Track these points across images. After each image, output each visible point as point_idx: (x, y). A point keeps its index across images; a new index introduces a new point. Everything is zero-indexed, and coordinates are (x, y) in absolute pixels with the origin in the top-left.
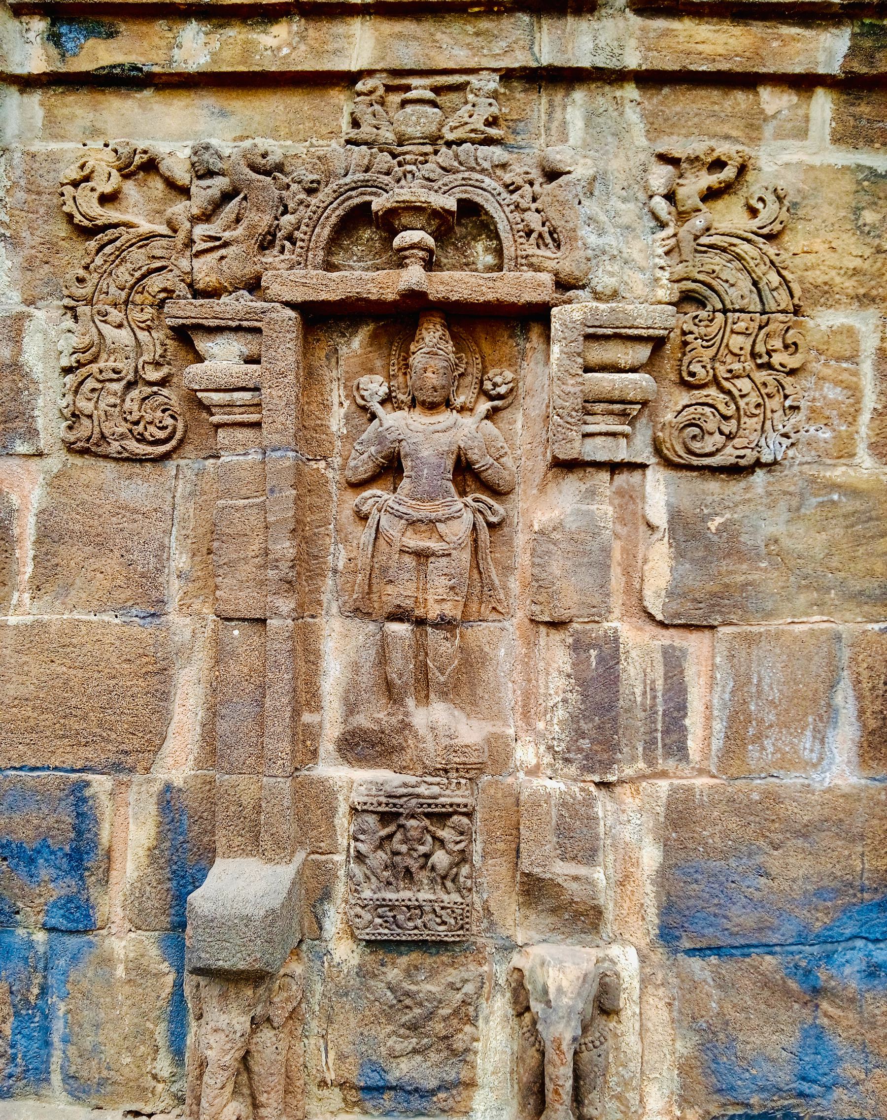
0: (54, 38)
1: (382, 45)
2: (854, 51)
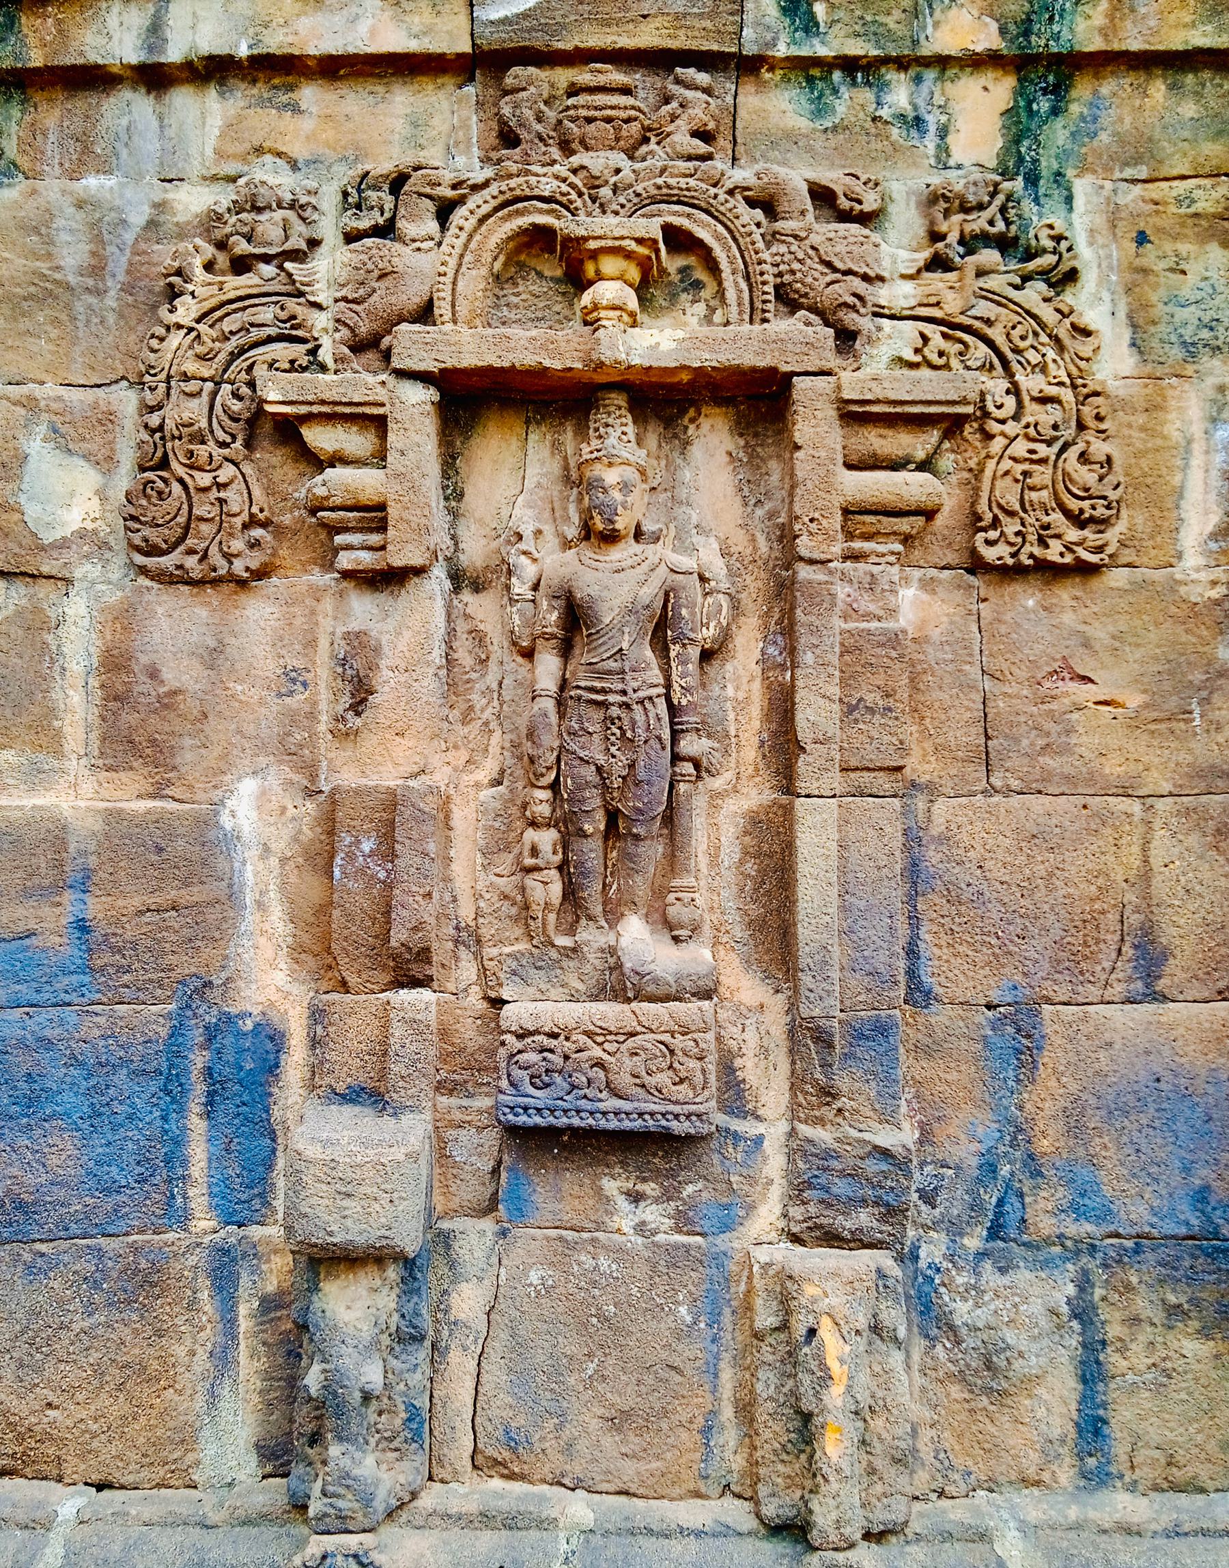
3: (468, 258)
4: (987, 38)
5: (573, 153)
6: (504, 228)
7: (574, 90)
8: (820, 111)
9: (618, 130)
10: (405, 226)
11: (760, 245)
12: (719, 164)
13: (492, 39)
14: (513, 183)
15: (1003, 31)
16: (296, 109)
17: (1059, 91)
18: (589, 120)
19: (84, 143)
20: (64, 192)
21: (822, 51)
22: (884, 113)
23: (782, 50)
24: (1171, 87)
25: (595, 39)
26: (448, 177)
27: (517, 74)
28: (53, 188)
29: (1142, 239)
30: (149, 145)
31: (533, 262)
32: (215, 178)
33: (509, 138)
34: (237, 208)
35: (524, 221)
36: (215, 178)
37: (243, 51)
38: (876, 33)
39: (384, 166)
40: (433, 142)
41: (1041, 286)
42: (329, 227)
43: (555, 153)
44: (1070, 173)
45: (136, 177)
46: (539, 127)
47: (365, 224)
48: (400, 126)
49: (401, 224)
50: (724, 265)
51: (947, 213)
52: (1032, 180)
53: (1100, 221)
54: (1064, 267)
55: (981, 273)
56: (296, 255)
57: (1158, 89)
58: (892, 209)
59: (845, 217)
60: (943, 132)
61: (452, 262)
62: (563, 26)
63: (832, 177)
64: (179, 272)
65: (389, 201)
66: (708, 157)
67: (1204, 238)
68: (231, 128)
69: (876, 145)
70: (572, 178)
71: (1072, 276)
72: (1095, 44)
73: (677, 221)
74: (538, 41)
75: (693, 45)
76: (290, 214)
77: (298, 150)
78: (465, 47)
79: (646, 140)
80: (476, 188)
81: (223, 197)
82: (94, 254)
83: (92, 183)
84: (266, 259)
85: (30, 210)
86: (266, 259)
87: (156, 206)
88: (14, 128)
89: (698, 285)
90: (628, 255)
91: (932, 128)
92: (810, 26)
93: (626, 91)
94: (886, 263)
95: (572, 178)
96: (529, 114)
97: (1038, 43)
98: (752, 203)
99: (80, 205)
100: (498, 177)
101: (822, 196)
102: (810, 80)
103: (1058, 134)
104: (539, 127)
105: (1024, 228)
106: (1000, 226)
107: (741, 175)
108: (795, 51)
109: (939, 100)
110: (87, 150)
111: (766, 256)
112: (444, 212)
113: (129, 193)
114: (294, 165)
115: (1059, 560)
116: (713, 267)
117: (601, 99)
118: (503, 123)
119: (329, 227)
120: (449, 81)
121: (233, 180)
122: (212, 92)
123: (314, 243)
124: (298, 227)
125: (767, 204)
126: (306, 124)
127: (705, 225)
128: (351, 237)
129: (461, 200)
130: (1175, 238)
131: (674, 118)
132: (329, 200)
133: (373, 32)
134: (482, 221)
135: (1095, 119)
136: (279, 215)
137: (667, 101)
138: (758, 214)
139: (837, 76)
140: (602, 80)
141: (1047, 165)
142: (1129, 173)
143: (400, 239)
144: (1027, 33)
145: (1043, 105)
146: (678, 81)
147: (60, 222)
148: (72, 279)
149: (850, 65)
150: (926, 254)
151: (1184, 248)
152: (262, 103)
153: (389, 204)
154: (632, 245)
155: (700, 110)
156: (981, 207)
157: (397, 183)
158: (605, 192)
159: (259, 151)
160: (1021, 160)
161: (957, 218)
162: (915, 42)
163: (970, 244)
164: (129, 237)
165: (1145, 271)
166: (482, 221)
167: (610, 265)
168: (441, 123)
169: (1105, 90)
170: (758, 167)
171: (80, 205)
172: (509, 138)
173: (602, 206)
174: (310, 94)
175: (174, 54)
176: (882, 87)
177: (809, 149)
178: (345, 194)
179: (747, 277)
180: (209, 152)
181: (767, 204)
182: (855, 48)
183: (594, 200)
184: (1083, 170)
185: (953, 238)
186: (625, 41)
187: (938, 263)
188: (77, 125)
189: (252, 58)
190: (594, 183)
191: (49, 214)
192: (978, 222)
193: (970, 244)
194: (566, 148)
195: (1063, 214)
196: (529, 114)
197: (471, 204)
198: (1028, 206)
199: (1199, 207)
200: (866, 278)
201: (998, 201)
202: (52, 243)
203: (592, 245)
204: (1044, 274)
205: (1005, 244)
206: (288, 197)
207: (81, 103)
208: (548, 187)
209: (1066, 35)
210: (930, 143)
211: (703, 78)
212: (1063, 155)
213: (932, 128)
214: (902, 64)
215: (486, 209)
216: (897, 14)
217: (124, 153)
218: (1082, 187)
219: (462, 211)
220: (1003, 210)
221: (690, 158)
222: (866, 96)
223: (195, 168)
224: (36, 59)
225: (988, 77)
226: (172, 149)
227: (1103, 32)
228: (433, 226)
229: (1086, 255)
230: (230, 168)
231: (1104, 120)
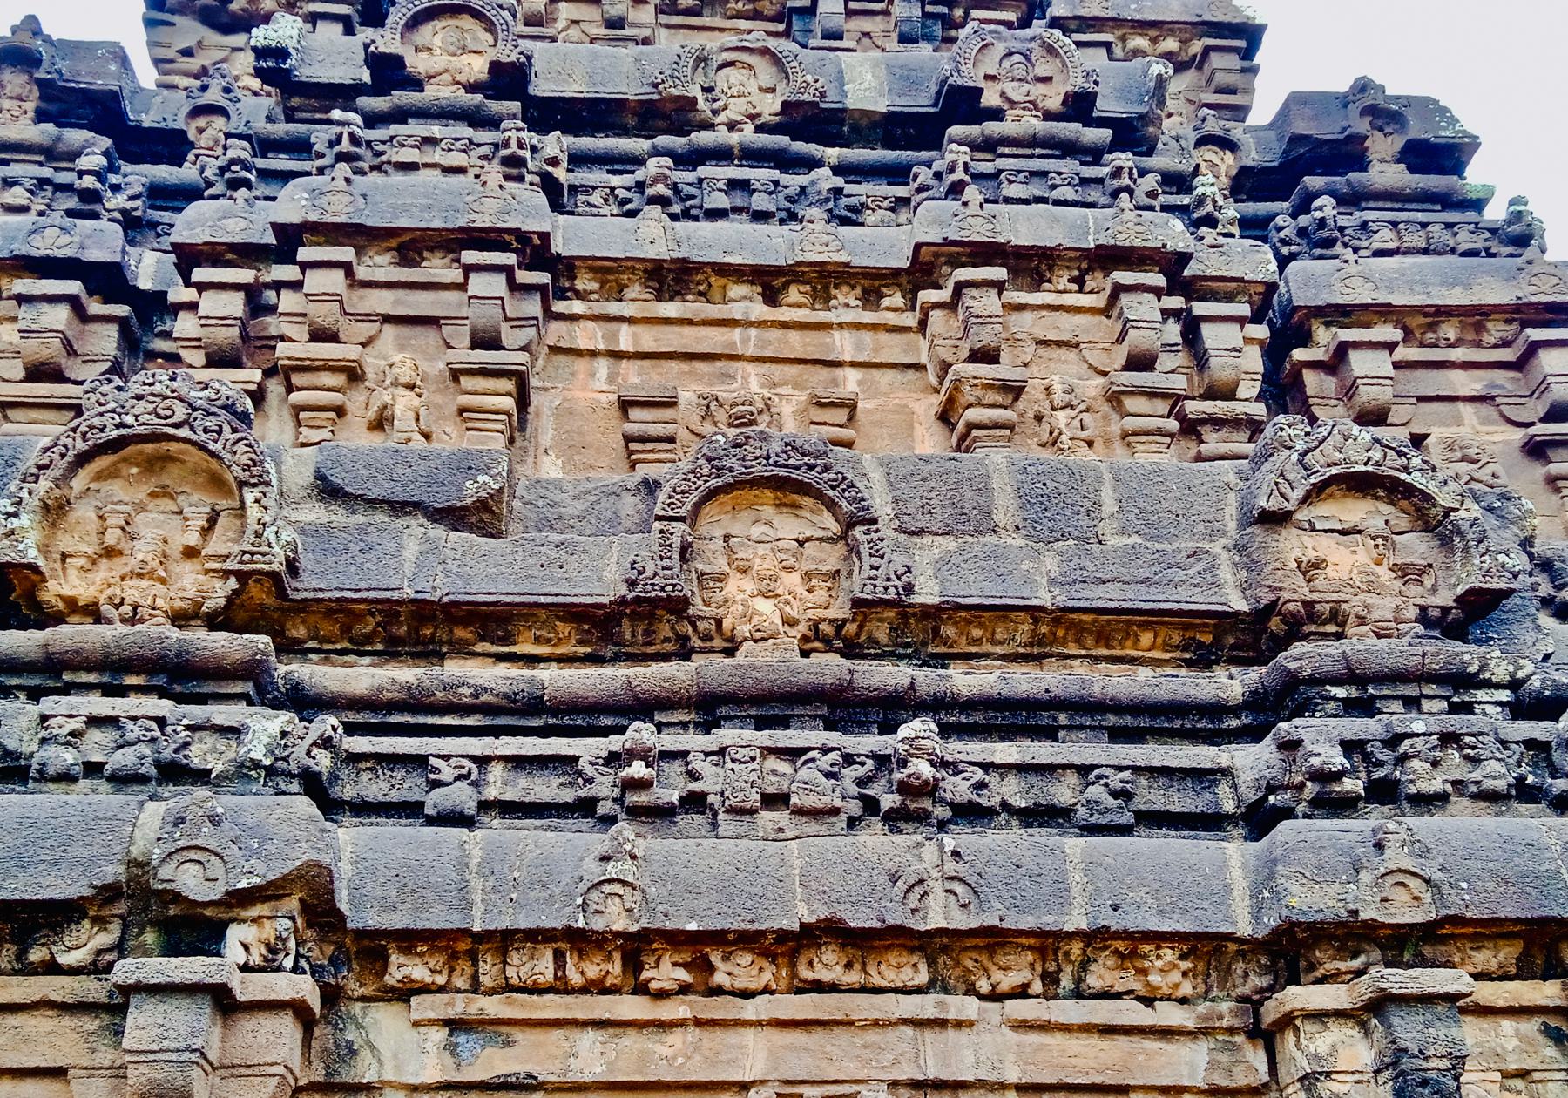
0: (452, 1049)
1: (772, 1053)
2: (1212, 1065)
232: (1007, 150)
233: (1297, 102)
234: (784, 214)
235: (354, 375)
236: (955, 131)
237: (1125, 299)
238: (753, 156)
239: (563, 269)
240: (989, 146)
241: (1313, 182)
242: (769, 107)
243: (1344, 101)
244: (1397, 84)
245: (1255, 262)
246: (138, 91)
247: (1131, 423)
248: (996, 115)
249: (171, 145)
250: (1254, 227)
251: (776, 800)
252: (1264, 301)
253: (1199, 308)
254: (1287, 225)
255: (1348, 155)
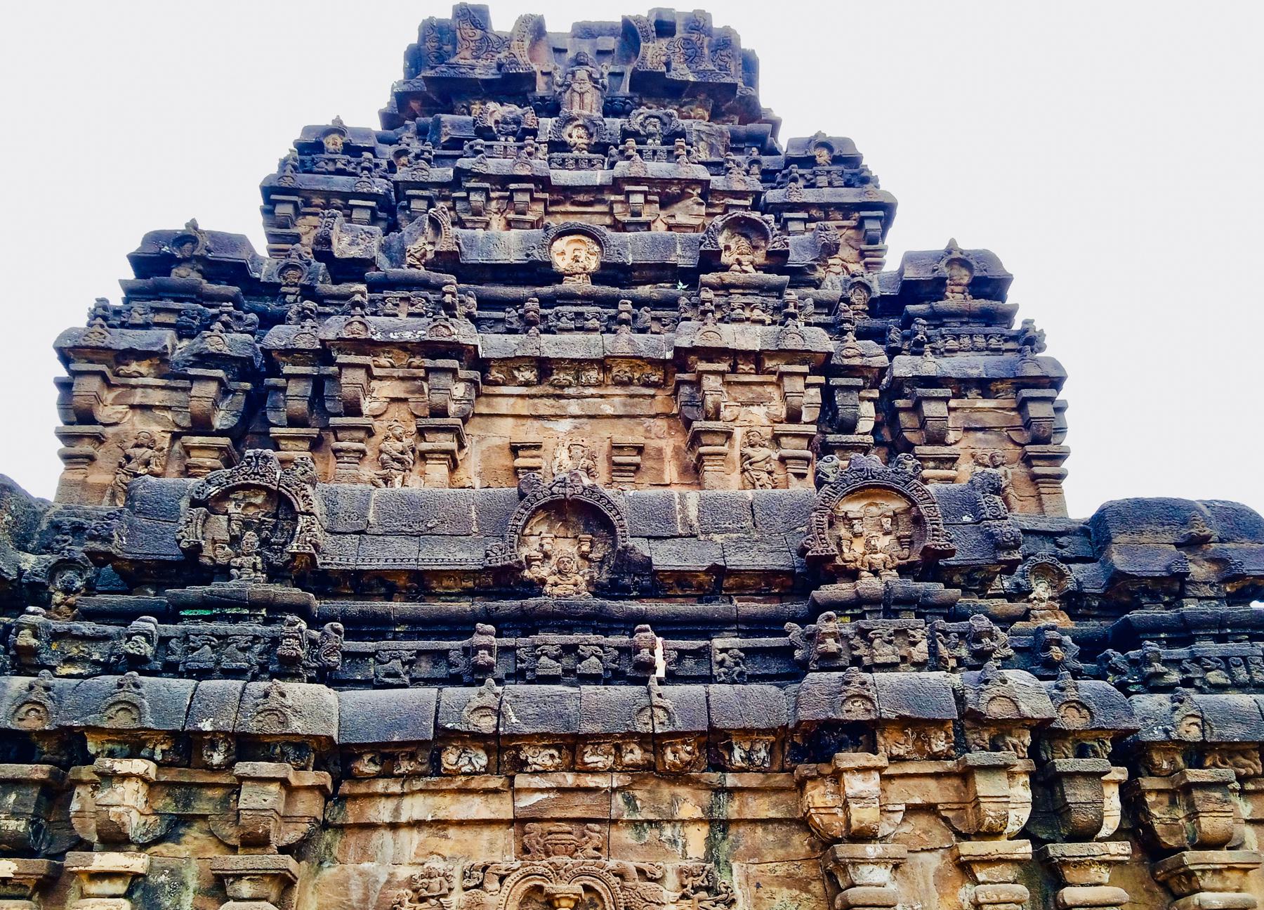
3: (510, 898)
4: (698, 814)
5: (550, 856)
6: (523, 887)
7: (550, 833)
8: (640, 837)
9: (566, 848)
10: (488, 886)
11: (619, 892)
12: (603, 861)
13: (520, 815)
14: (528, 868)
15: (703, 811)
16: (446, 837)
17: (724, 831)
18: (556, 844)
19: (364, 850)
20: (355, 869)
21: (640, 818)
22: (663, 838)
23: (625, 817)
24: (764, 829)
25: (558, 814)
26: (504, 866)
27: (530, 826)
28: (350, 868)
29: (758, 886)
30: (390, 851)
31: (534, 896)
32: (414, 864)
33: (526, 850)
34: (422, 877)
35: (532, 883)
36: (414, 864)
37: (429, 818)
38: (657, 810)
39: (480, 863)
40: (497, 850)
41: (722, 906)
42: (457, 883)
43: (543, 856)
44: (731, 861)
45: (383, 863)
46: (537, 847)
47: (472, 884)
48: (485, 844)
49: (486, 885)
50: (606, 900)
51: (687, 877)
52: (717, 863)
53: (743, 879)
54: (730, 898)
55: (700, 901)
56: (444, 896)
57: (759, 830)
58: (667, 875)
59: (650, 880)
60: (684, 846)
61: (505, 900)
62: (547, 810)
63: (646, 867)
64: (399, 903)
65: (481, 875)
66: (599, 858)
67: (781, 885)
68: (422, 845)
69: (661, 850)
70: (550, 867)
71: (733, 901)
72: (735, 816)
73: (588, 883)
74: (538, 815)
75: (594, 816)
76: (442, 878)
77: (447, 854)
78: (511, 817)
79: (576, 850)
80: (514, 871)
81: (417, 872)
82: (364, 894)
83: (366, 865)
84: (433, 897)
85: (341, 877)
86: (433, 897)
87: (390, 874)
88: (338, 844)
89: (596, 906)
90: (570, 899)
91: (680, 844)
92: (635, 809)
93: (570, 833)
94: (665, 898)
95: (550, 867)
96: (534, 842)
97: (716, 815)
98: (615, 875)
99: (360, 874)
100: (523, 866)
101: (641, 872)
102: (636, 826)
103: (725, 846)
104: (537, 847)
105: (715, 883)
106: (706, 883)
107: (612, 864)
108: (629, 818)
109: (682, 834)
110: (365, 852)
111: (621, 896)
112: (502, 879)
113: (380, 870)
114: (444, 859)
115: (867, 717)
116: (602, 899)
117: (560, 836)
118: (524, 845)
119: (457, 883)
120: (504, 827)
121: (423, 864)
122: (415, 831)
123: (450, 890)
124: (446, 884)
125: (621, 875)
126: (450, 843)
127: (597, 884)
128: (466, 889)
129: (509, 875)
130: (770, 885)
131: (587, 843)
132: (457, 873)
133: (478, 812)
134: (516, 883)
135: (738, 841)
136: (439, 879)
137: (584, 836)
138: (618, 879)
139: (645, 825)
140: (561, 829)
141: (722, 858)
142: (751, 861)
143: (485, 890)
144: (711, 812)
145: (719, 836)
146: (588, 829)
147: (352, 881)
148: (355, 904)
149: (650, 822)
150: (679, 894)
151: (774, 889)
152: (433, 835)
153: (481, 877)
154: (572, 896)
155: (597, 840)
156: (699, 875)
157: (485, 868)
158: (562, 872)
159: (432, 853)
160: (713, 856)
161: (691, 879)
162: (672, 815)
163: (696, 889)
164: (379, 887)
165: (761, 898)
166: (516, 883)
167: (564, 903)
168: (500, 843)
169: (741, 830)
170: (618, 861)
171: (360, 874)
172: (526, 850)
173: (561, 878)
174: (452, 832)
175: (403, 819)
176: (661, 829)
177: (636, 851)
178: (465, 873)
179: (614, 904)
180: (413, 854)
181: (621, 875)
182: (652, 817)
183: (558, 874)
184: (735, 860)
185: (690, 886)
186: (569, 815)
187: (684, 897)
188: (362, 843)
189: (432, 821)
190: (557, 868)
191: (348, 878)
192: (698, 882)
193: (696, 889)
194: (548, 854)
195: (729, 877)
196: (534, 842)
197: (512, 877)
198: (716, 874)
199: (778, 873)
200: (658, 904)
201: (705, 872)
202: (348, 890)
203: (558, 896)
204: (723, 901)
205: (708, 889)
206: (442, 872)
207: (364, 834)
208: (541, 870)
209: (725, 813)
210: (680, 849)
211: (597, 827)
212: (728, 855)
213: (680, 844)
214: (669, 821)
215: (518, 879)
216: (666, 805)
217: (379, 854)
218: (735, 866)
219: (508, 879)
220: (707, 876)
221: (593, 858)
222: (656, 832)
223: (406, 860)
224: (351, 820)
225: (699, 826)
226: (399, 851)
227: (739, 812)
228: (497, 885)
229: (738, 894)
230: (420, 860)
231: (741, 842)
232: (329, 302)
233: (910, 258)
234: (604, 329)
235: (370, 432)
236: (704, 278)
237: (786, 380)
238: (589, 299)
239: (483, 365)
240: (726, 287)
241: (911, 308)
242: (593, 265)
243: (938, 257)
244: (967, 244)
245: (875, 355)
246: (255, 257)
247: (784, 452)
248: (726, 268)
249: (272, 290)
250: (878, 336)
251: (904, 659)
252: (874, 376)
253: (835, 381)
254: (895, 335)
255: (936, 288)
